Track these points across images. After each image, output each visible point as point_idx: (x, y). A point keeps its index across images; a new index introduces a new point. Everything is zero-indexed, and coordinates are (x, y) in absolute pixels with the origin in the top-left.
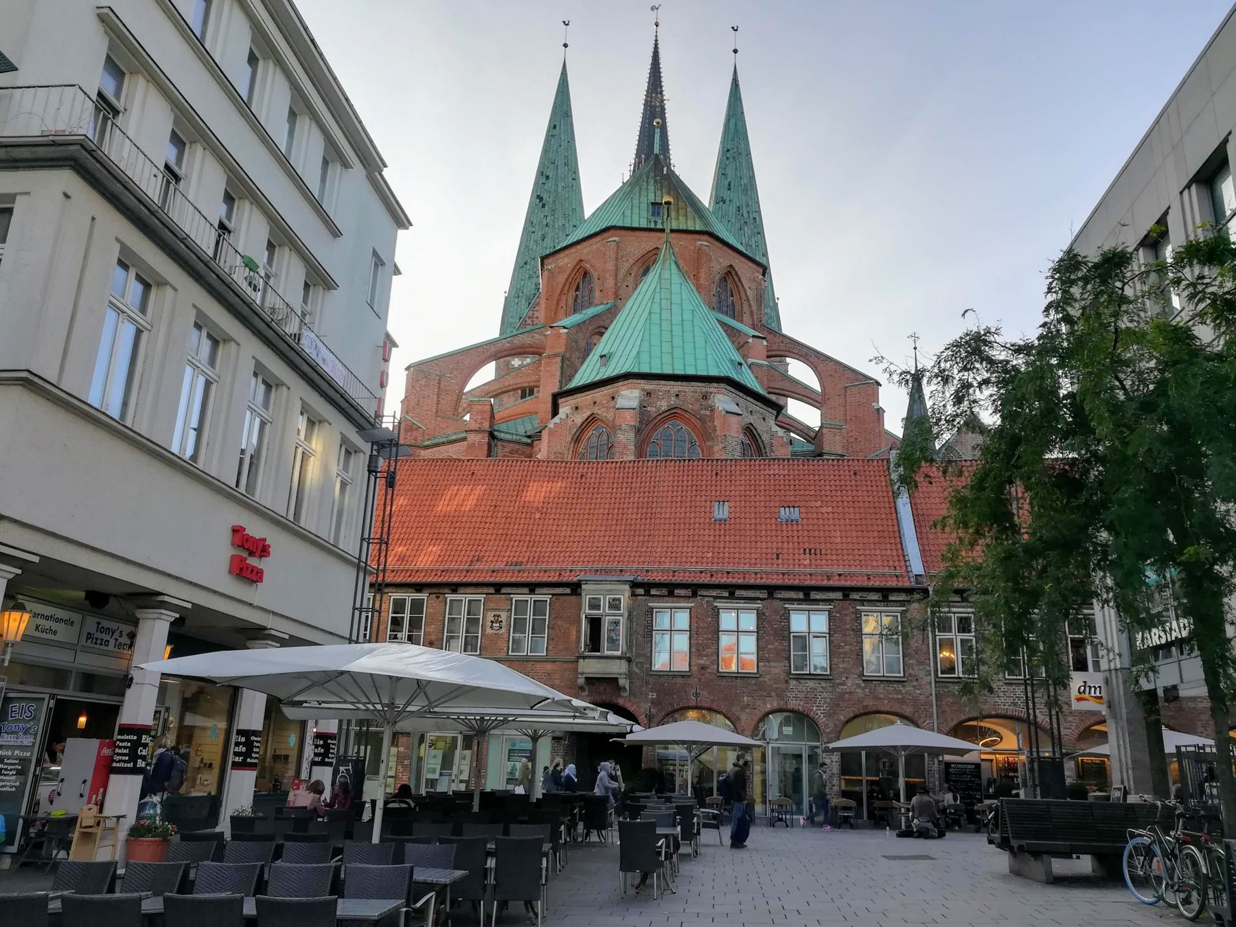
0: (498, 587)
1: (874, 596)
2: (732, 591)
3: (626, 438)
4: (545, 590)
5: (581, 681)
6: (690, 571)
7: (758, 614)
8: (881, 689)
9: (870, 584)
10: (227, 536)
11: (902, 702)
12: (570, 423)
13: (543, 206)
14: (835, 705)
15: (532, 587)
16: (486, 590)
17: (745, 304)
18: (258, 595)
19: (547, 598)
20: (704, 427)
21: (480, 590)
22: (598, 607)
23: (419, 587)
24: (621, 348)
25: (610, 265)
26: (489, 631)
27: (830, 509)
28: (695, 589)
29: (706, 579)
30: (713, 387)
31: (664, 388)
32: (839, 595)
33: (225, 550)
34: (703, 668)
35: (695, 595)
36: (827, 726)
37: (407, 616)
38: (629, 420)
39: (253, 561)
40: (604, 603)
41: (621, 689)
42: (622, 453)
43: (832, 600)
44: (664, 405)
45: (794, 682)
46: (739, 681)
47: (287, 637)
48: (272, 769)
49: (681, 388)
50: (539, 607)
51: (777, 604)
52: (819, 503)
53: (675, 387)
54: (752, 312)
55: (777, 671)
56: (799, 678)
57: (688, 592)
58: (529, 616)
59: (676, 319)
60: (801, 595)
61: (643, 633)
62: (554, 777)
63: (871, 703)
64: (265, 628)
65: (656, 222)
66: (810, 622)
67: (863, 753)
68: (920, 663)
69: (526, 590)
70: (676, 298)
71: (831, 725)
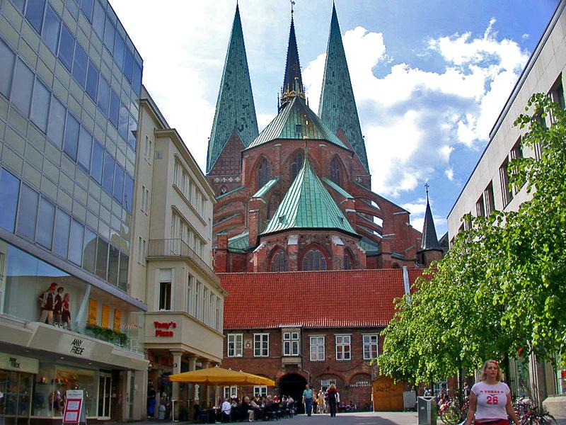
3: (293, 258)
5: (283, 366)
12: (266, 249)
13: (229, 89)
17: (344, 172)
19: (268, 334)
20: (328, 251)
24: (289, 213)
25: (278, 159)
26: (245, 347)
30: (330, 233)
34: (330, 359)
38: (293, 250)
40: (291, 336)
41: (298, 368)
44: (309, 242)
48: (159, 407)
50: (265, 338)
53: (314, 233)
54: (348, 176)
59: (313, 198)
61: (305, 347)
62: (389, 375)
65: (299, 135)
67: (197, 387)
70: (312, 187)
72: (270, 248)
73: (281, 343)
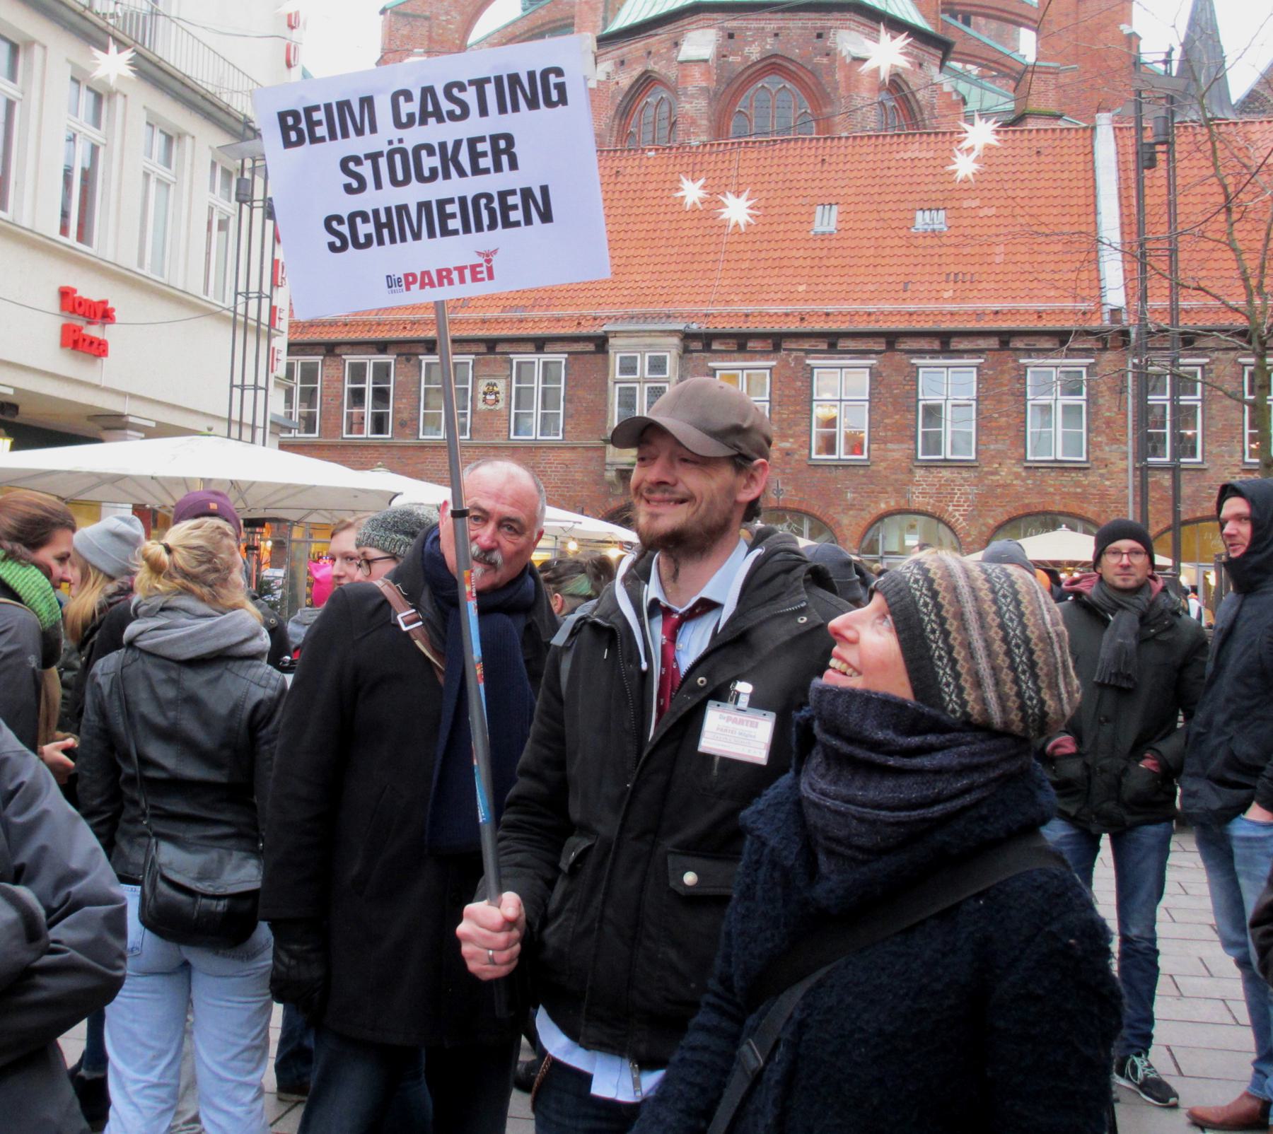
0: (491, 344)
1: (1046, 344)
2: (832, 342)
3: (694, 107)
4: (558, 347)
5: (611, 475)
6: (772, 312)
7: (871, 374)
8: (1052, 480)
9: (1040, 325)
10: (53, 303)
11: (1082, 497)
14: (983, 503)
15: (540, 344)
16: (474, 348)
18: (108, 371)
19: (562, 358)
21: (467, 349)
22: (632, 370)
23: (382, 347)
26: (481, 406)
27: (993, 211)
28: (776, 341)
29: (793, 326)
31: (754, 25)
32: (993, 343)
33: (51, 323)
35: (777, 348)
36: (968, 535)
37: (369, 387)
38: (697, 80)
39: (94, 331)
40: (643, 365)
42: (688, 134)
43: (981, 351)
44: (754, 52)
45: (919, 473)
46: (840, 472)
47: (153, 424)
49: (782, 24)
51: (898, 357)
52: (977, 203)
55: (897, 455)
56: (928, 466)
57: (768, 345)
58: (538, 385)
60: (936, 345)
63: (1035, 502)
64: (121, 416)
66: (949, 386)
68: (1115, 440)
69: (531, 347)
71: (974, 532)
72: (626, 80)
73: (604, 390)
